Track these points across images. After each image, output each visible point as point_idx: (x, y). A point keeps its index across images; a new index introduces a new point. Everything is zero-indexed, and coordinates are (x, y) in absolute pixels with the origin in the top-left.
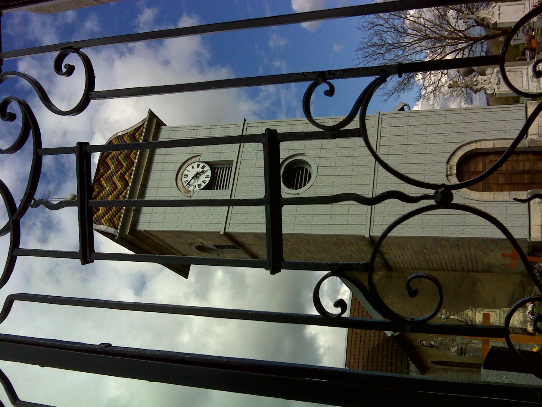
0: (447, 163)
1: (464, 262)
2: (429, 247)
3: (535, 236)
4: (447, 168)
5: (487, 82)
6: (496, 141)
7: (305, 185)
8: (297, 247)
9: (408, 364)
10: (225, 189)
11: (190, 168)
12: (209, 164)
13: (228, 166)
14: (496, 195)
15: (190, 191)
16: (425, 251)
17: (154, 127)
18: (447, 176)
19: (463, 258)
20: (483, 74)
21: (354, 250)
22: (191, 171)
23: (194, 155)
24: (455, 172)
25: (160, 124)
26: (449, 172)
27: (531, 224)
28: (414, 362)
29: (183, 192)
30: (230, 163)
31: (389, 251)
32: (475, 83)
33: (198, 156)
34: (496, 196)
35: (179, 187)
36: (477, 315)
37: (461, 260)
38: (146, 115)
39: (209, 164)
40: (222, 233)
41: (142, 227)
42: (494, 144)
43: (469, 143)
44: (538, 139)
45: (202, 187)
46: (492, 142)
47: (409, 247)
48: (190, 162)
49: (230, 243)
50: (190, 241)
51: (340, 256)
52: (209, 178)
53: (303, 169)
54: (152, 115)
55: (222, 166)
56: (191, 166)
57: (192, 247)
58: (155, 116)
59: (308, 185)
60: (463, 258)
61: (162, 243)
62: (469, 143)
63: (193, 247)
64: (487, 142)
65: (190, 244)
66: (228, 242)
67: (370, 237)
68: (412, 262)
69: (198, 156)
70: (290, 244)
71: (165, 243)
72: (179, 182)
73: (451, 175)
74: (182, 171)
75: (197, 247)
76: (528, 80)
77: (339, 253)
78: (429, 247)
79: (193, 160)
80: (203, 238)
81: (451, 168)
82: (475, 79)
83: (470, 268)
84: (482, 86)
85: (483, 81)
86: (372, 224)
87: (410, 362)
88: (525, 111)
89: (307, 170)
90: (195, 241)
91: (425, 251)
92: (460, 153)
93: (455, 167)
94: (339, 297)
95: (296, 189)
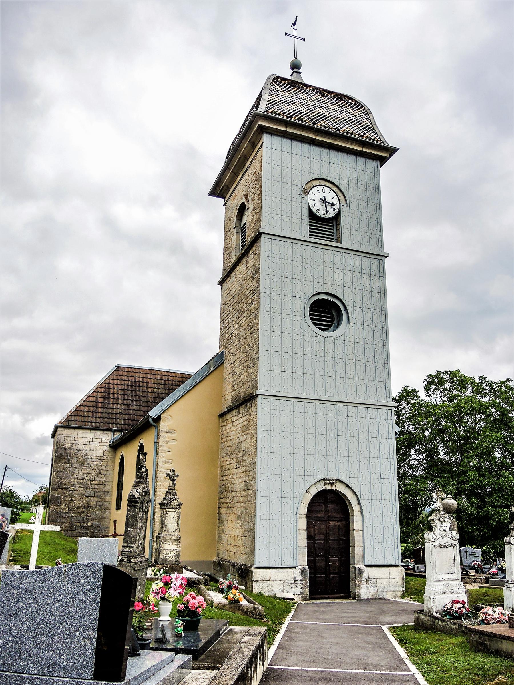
0: (338, 480)
1: (229, 494)
2: (246, 458)
3: (258, 573)
4: (333, 480)
5: (443, 533)
6: (361, 532)
7: (315, 324)
8: (244, 315)
9: (121, 431)
10: (310, 235)
11: (333, 194)
12: (337, 217)
13: (335, 238)
14: (303, 531)
15: (307, 195)
16: (241, 454)
17: (379, 153)
18: (324, 480)
19: (233, 494)
20: (451, 529)
21: (241, 377)
22: (331, 196)
23: (347, 199)
24: (328, 487)
25: (382, 161)
26: (328, 482)
27: (271, 570)
28: (121, 438)
29: (307, 186)
30: (338, 240)
31: (241, 415)
32: (442, 519)
33: (346, 203)
34: (302, 532)
35: (312, 182)
36: (174, 510)
37: (231, 492)
38: (392, 144)
39: (337, 217)
40: (261, 230)
41: (266, 139)
42: (358, 530)
43: (359, 503)
44: (364, 578)
45: (312, 208)
46: (360, 528)
47: (245, 437)
48: (340, 194)
49: (248, 240)
50: (251, 196)
51: (234, 362)
52: (322, 216)
53: (332, 322)
54: (392, 151)
55: (335, 231)
56: (335, 195)
57: (244, 198)
58: (391, 155)
59: (315, 328)
60: (233, 494)
61: (247, 165)
62: (359, 503)
63: (244, 200)
64: (360, 523)
65: (247, 196)
66: (250, 238)
67: (257, 396)
68: (228, 439)
69: (346, 203)
70: (248, 307)
71: (248, 168)
72: (317, 183)
73: (326, 484)
74: (330, 185)
75: (243, 204)
76: (444, 580)
77: (238, 361)
78: (246, 458)
79: (342, 198)
80: (254, 210)
81: (332, 484)
82: (446, 519)
83: (223, 500)
84: (439, 528)
85: (444, 528)
86: (271, 397)
87: (123, 433)
88: (394, 564)
89: (330, 326)
90: (250, 202)
91: (241, 454)
92: (348, 494)
93: (333, 488)
94: (396, 390)
95: (310, 314)
